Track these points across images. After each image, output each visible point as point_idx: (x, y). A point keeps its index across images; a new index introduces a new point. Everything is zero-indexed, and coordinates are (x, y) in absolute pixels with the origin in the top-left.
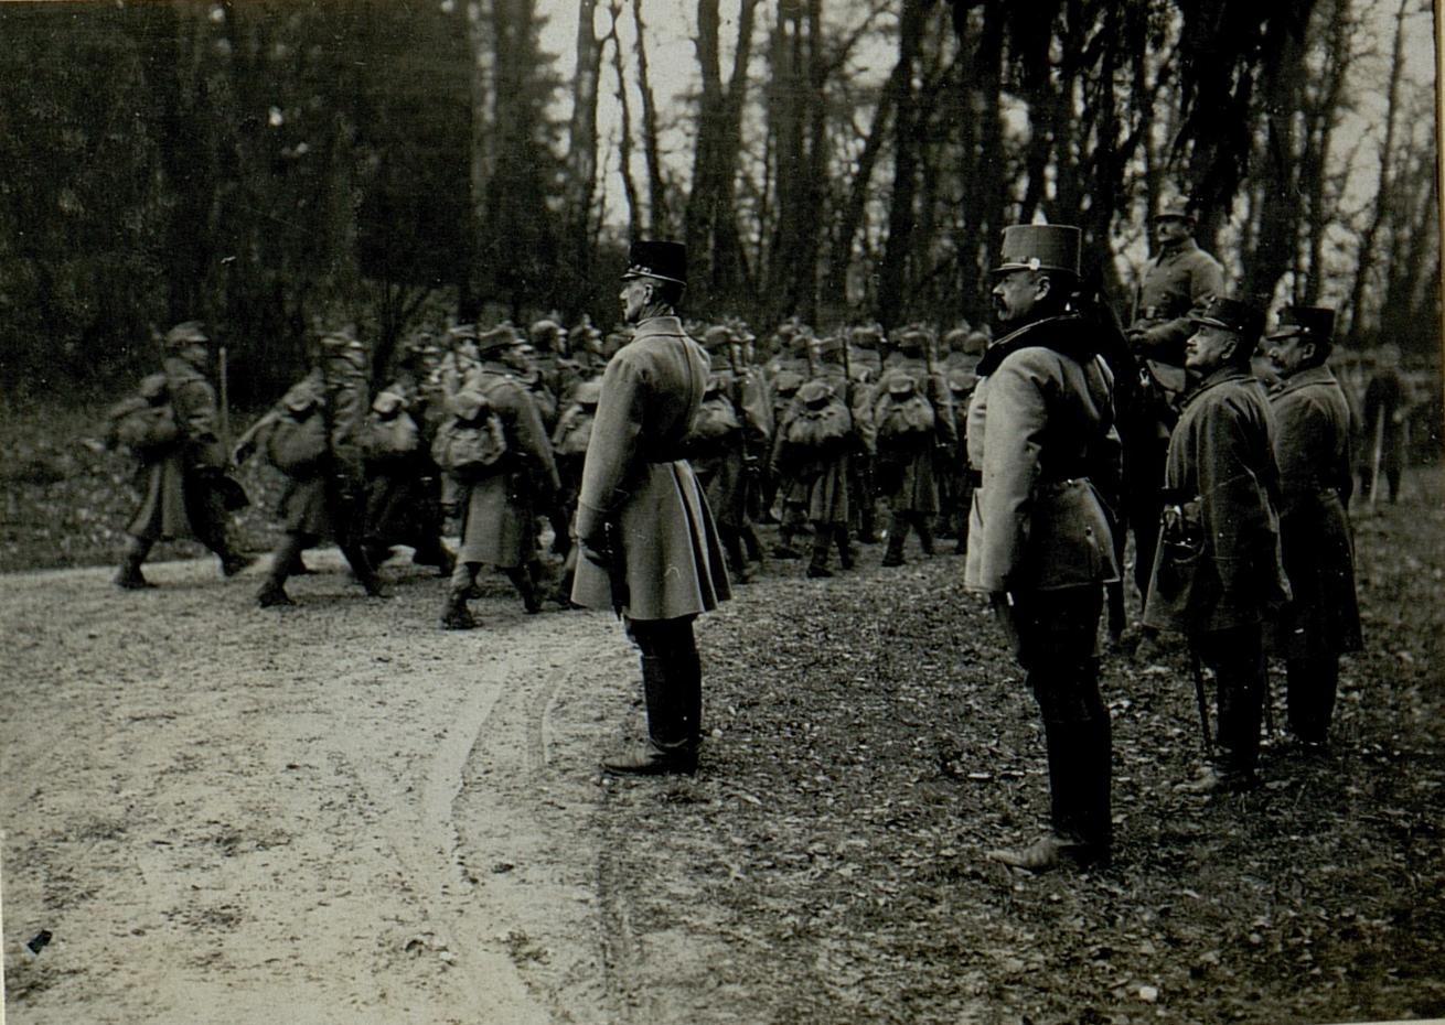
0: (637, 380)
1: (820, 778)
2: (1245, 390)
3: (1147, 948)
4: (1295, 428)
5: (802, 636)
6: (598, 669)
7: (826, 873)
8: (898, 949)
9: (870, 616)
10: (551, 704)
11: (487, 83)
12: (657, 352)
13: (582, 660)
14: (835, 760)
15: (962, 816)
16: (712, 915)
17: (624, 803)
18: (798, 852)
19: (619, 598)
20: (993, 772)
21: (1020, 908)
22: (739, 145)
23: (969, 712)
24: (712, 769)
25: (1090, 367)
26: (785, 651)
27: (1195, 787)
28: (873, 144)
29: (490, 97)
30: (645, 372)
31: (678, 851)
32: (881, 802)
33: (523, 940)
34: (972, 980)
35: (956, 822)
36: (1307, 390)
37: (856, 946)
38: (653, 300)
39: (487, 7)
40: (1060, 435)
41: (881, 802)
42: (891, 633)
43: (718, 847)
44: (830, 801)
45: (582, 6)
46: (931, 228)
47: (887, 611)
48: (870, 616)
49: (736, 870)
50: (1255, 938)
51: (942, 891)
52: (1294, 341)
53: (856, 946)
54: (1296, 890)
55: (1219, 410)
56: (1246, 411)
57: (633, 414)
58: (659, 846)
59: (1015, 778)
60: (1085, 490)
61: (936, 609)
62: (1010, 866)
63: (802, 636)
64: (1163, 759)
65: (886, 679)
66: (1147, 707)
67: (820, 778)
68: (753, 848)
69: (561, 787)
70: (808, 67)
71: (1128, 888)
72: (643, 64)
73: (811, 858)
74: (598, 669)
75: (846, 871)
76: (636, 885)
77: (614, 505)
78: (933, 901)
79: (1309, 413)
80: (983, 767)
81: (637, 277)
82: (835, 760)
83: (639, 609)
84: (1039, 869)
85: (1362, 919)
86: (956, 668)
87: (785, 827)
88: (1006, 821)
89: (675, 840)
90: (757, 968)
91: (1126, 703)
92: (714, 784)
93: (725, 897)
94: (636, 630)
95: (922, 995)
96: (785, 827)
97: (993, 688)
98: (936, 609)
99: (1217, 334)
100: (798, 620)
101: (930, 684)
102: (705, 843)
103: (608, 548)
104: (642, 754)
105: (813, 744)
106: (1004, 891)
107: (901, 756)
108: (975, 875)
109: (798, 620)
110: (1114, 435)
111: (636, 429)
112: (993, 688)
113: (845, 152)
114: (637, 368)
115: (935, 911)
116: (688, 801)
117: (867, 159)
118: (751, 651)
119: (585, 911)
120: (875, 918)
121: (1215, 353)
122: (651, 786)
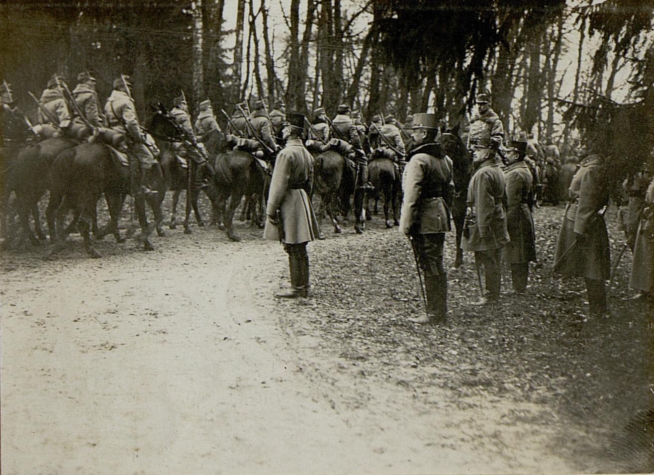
0: (288, 160)
1: (350, 299)
2: (492, 169)
3: (456, 343)
4: (514, 182)
5: (339, 258)
6: (266, 267)
7: (353, 324)
8: (378, 342)
9: (364, 252)
10: (252, 278)
11: (201, 41)
12: (295, 151)
13: (265, 259)
14: (354, 295)
15: (398, 310)
16: (318, 333)
17: (283, 305)
18: (344, 318)
19: (282, 236)
20: (409, 299)
21: (416, 333)
22: (307, 64)
23: (401, 281)
24: (312, 296)
25: (442, 161)
26: (334, 262)
27: (477, 304)
28: (362, 62)
29: (201, 41)
30: (291, 158)
31: (304, 317)
32: (371, 306)
33: (259, 338)
34: (400, 349)
35: (396, 312)
36: (518, 169)
37: (364, 341)
38: (292, 134)
39: (200, 4)
40: (429, 184)
41: (371, 306)
42: (373, 257)
43: (318, 317)
44: (353, 306)
45: (239, 4)
46: (387, 99)
47: (371, 250)
48: (364, 252)
49: (324, 322)
50: (490, 341)
51: (391, 329)
52: (512, 153)
53: (364, 341)
54: (506, 330)
55: (482, 175)
56: (492, 176)
57: (287, 172)
58: (299, 316)
59: (417, 301)
60: (439, 202)
61: (389, 250)
62: (413, 322)
63: (339, 258)
64: (468, 296)
65: (371, 272)
66: (464, 282)
67: (350, 299)
68: (329, 317)
69: (262, 301)
70: (332, 29)
71: (450, 328)
72: (266, 29)
73: (348, 320)
74: (266, 267)
75: (360, 323)
76: (292, 326)
77: (281, 203)
78: (388, 331)
79: (518, 177)
80: (405, 297)
81: (287, 126)
82: (354, 295)
83: (289, 240)
84: (423, 324)
85: (526, 338)
86: (396, 269)
87: (340, 313)
88: (413, 312)
89: (303, 315)
90: (334, 345)
91: (457, 280)
92: (314, 300)
93: (322, 329)
94: (288, 248)
95: (385, 352)
96: (340, 313)
97: (410, 275)
98: (389, 250)
99: (483, 151)
100: (337, 253)
101: (387, 273)
102: (313, 315)
103: (278, 218)
104: (289, 292)
105: (346, 290)
106: (411, 328)
107: (377, 294)
108: (402, 325)
109: (337, 253)
110: (452, 183)
111: (288, 177)
112: (410, 275)
113: (350, 63)
114: (288, 156)
115: (389, 334)
116: (306, 305)
117: (359, 70)
118: (320, 262)
119: (276, 332)
120: (370, 335)
121: (483, 156)
122: (292, 301)
